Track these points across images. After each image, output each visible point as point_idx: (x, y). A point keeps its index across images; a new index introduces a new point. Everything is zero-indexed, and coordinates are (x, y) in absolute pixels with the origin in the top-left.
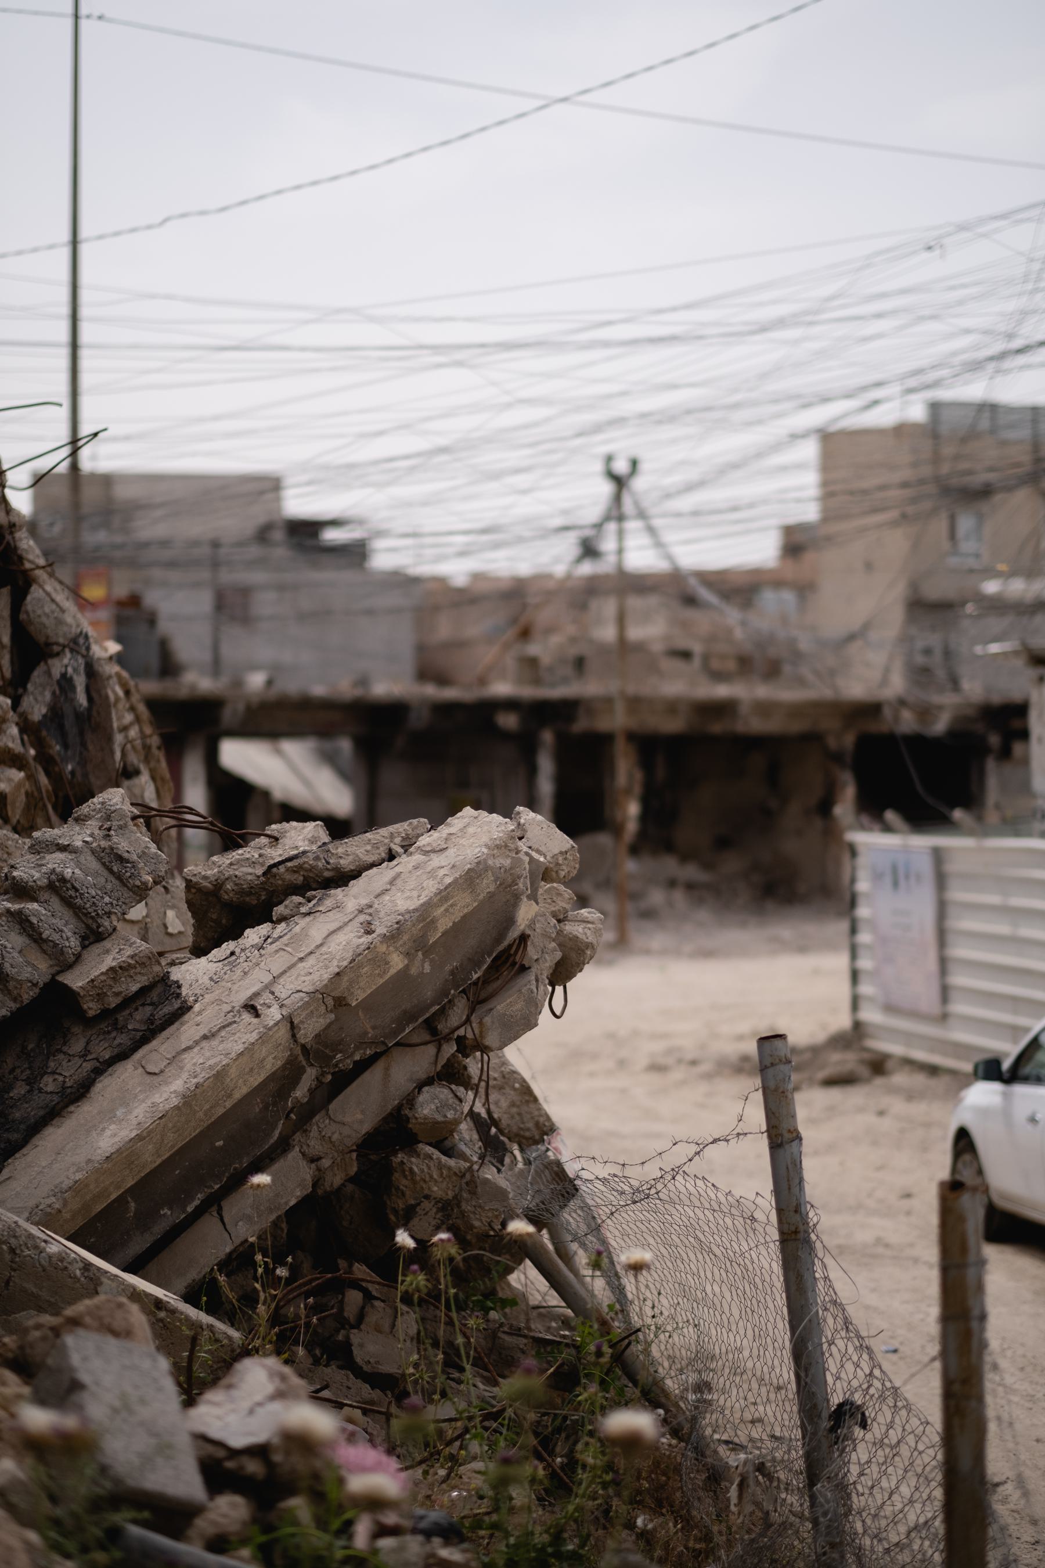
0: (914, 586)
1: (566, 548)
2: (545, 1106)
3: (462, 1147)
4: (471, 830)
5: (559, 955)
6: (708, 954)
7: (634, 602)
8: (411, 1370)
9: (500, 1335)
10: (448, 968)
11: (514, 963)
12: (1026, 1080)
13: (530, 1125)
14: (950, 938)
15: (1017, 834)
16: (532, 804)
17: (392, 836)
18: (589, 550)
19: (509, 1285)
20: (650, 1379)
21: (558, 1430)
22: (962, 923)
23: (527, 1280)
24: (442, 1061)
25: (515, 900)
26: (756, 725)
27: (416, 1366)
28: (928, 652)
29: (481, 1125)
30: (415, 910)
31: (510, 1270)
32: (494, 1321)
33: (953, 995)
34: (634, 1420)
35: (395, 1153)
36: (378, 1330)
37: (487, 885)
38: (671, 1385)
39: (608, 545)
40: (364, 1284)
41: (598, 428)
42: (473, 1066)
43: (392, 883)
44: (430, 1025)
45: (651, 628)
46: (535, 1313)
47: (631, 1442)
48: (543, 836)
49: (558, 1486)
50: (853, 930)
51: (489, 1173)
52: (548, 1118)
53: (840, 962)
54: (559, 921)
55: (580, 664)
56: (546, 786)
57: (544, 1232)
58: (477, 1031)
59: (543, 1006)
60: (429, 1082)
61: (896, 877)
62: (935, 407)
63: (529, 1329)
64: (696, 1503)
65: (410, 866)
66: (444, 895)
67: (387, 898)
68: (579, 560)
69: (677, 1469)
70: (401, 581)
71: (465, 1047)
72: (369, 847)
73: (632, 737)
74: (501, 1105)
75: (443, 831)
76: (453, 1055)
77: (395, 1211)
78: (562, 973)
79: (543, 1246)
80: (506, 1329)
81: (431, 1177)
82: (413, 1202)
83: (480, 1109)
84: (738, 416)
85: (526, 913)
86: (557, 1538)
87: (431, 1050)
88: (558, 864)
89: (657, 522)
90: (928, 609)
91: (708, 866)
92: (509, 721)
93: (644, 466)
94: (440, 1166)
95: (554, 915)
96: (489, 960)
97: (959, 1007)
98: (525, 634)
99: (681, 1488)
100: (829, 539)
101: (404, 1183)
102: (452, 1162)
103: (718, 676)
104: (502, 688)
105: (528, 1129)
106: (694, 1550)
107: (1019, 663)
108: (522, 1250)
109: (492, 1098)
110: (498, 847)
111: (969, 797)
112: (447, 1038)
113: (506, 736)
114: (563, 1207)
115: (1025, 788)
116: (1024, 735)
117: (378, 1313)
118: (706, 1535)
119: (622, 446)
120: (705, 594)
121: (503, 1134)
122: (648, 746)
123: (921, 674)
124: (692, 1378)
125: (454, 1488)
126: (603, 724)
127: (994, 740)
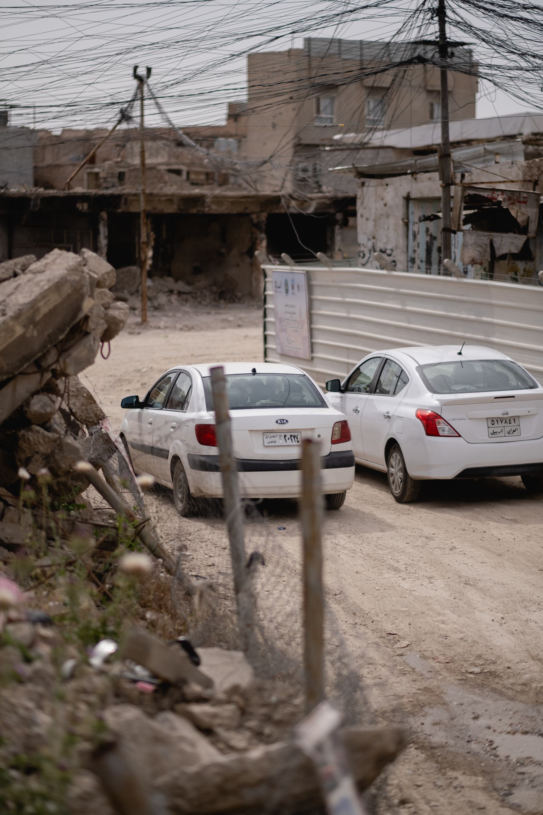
0: (297, 136)
1: (113, 113)
2: (100, 406)
3: (56, 426)
4: (58, 261)
5: (105, 326)
6: (190, 329)
7: (149, 144)
8: (28, 541)
9: (77, 523)
10: (46, 333)
11: (82, 331)
12: (352, 390)
13: (92, 415)
14: (315, 318)
15: (351, 266)
16: (96, 249)
17: (16, 265)
18: (125, 116)
19: (82, 498)
20: (155, 544)
21: (107, 571)
22: (321, 310)
23: (91, 495)
24: (44, 382)
25: (82, 298)
26: (215, 209)
27: (31, 538)
28: (305, 170)
29: (66, 415)
30: (29, 303)
31: (82, 490)
32: (73, 516)
33: (316, 348)
34: (138, 560)
35: (20, 430)
36: (12, 521)
37: (67, 290)
38: (166, 547)
39: (136, 113)
40: (4, 498)
41: (128, 51)
42: (61, 384)
43: (16, 288)
44: (38, 363)
45: (159, 159)
46: (95, 513)
47: (137, 572)
48: (97, 264)
49: (106, 598)
50: (265, 316)
51: (70, 440)
52: (102, 412)
53: (259, 332)
54: (106, 309)
55: (121, 176)
56: (103, 242)
57: (101, 470)
58: (62, 366)
59: (97, 352)
60: (37, 392)
61: (287, 288)
62: (308, 41)
63: (92, 520)
64: (179, 607)
65: (25, 280)
66: (44, 295)
67: (13, 297)
68: (120, 122)
69: (169, 590)
70: (24, 131)
71: (56, 375)
72: (3, 270)
73: (148, 215)
74: (76, 405)
75: (43, 261)
76: (50, 379)
77: (20, 460)
78: (107, 336)
79: (98, 477)
80: (80, 520)
81: (39, 442)
82: (29, 455)
83: (64, 406)
84: (202, 45)
85: (88, 305)
86: (104, 624)
87: (38, 376)
88: (105, 279)
89: (160, 101)
90: (304, 148)
91: (189, 283)
92: (83, 207)
93: (153, 71)
94: (44, 437)
95: (103, 305)
96: (68, 329)
97: (319, 354)
98: (92, 161)
99: (171, 599)
100: (253, 110)
101: (24, 445)
102: (50, 435)
103: (195, 184)
104: (79, 190)
105: (91, 418)
106: (178, 630)
107: (351, 175)
108: (87, 479)
109: (71, 402)
110: (72, 270)
111: (326, 246)
112: (46, 370)
113: (81, 214)
114: (110, 457)
115: (355, 241)
116: (354, 214)
117: (11, 513)
118: (184, 623)
119: (143, 61)
120: (187, 140)
121: (78, 420)
122: (157, 220)
123: (301, 183)
124: (177, 544)
125: (51, 600)
126: (133, 209)
127: (339, 216)
